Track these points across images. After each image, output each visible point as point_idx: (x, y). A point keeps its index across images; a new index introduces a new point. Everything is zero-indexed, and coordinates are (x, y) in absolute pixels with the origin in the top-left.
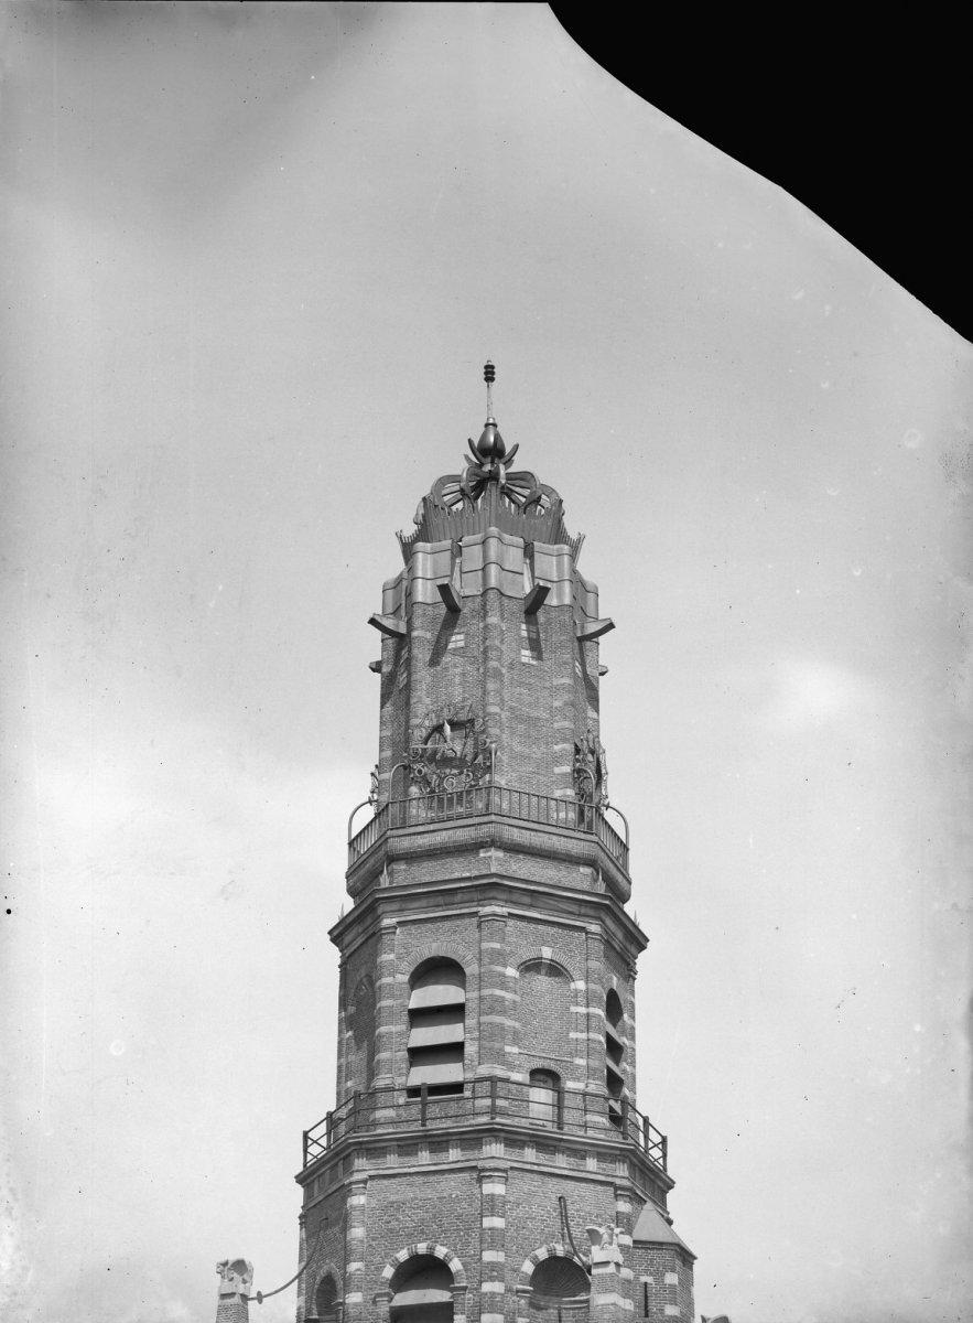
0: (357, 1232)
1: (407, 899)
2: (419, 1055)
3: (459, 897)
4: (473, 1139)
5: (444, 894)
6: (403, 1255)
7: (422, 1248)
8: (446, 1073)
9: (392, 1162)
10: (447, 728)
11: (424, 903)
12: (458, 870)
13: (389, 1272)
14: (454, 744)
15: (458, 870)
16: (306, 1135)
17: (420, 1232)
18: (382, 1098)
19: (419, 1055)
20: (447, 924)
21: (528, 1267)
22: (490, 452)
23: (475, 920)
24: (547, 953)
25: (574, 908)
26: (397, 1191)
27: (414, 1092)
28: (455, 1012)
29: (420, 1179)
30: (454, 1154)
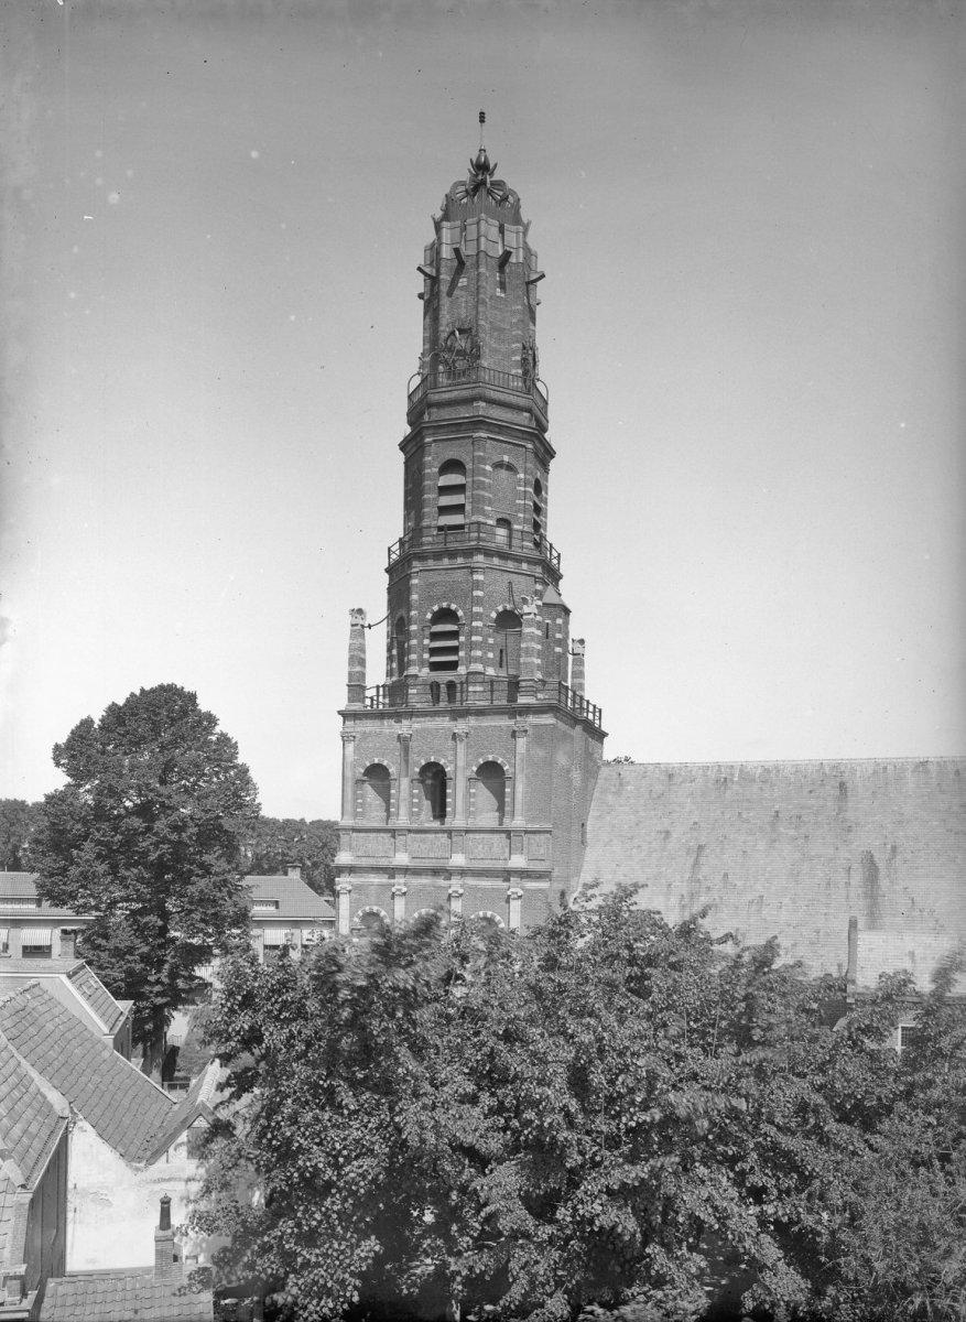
0: (415, 597)
1: (438, 428)
2: (444, 510)
3: (463, 427)
4: (469, 553)
5: (456, 426)
6: (436, 608)
8: (457, 519)
9: (431, 563)
10: (457, 332)
11: (446, 430)
12: (464, 412)
13: (429, 616)
14: (462, 343)
15: (464, 412)
16: (389, 549)
17: (445, 598)
18: (425, 531)
19: (444, 510)
20: (458, 442)
21: (494, 615)
22: (482, 167)
23: (471, 440)
24: (506, 458)
25: (520, 435)
26: (434, 578)
27: (440, 528)
28: (460, 489)
29: (444, 572)
30: (460, 560)
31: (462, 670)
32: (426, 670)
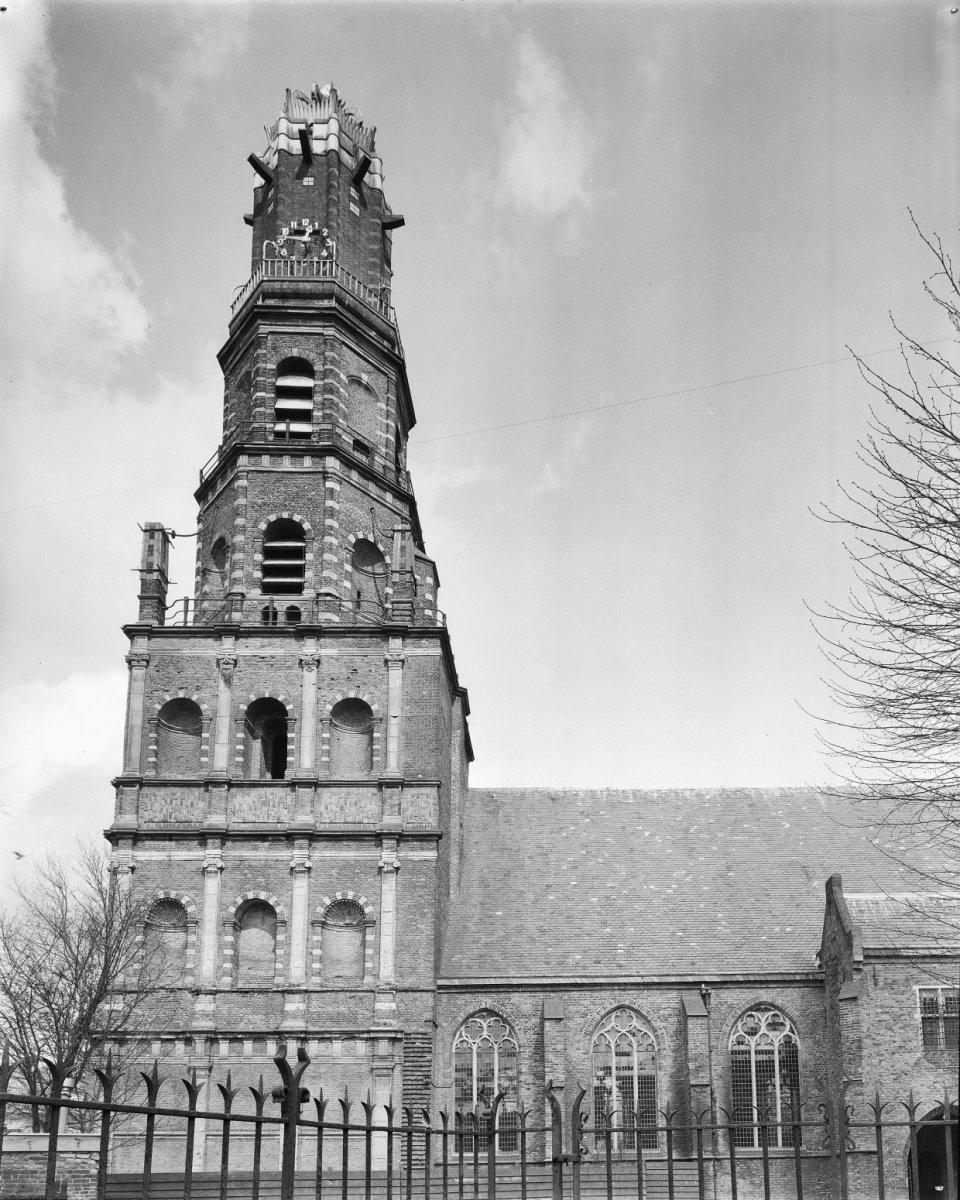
6: (273, 518)
7: (285, 515)
17: (266, 888)
31: (308, 593)
32: (256, 593)
